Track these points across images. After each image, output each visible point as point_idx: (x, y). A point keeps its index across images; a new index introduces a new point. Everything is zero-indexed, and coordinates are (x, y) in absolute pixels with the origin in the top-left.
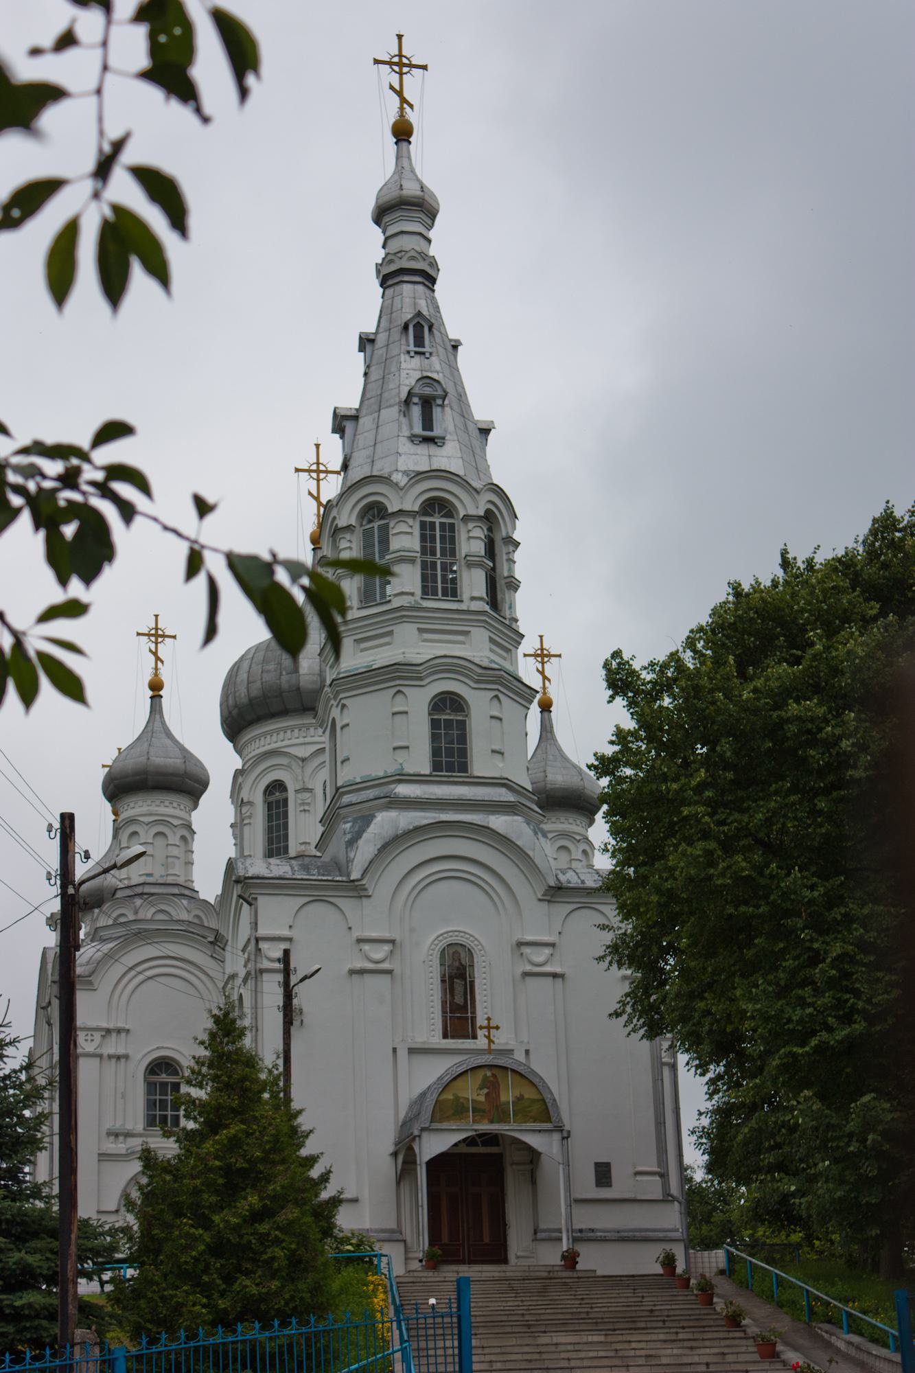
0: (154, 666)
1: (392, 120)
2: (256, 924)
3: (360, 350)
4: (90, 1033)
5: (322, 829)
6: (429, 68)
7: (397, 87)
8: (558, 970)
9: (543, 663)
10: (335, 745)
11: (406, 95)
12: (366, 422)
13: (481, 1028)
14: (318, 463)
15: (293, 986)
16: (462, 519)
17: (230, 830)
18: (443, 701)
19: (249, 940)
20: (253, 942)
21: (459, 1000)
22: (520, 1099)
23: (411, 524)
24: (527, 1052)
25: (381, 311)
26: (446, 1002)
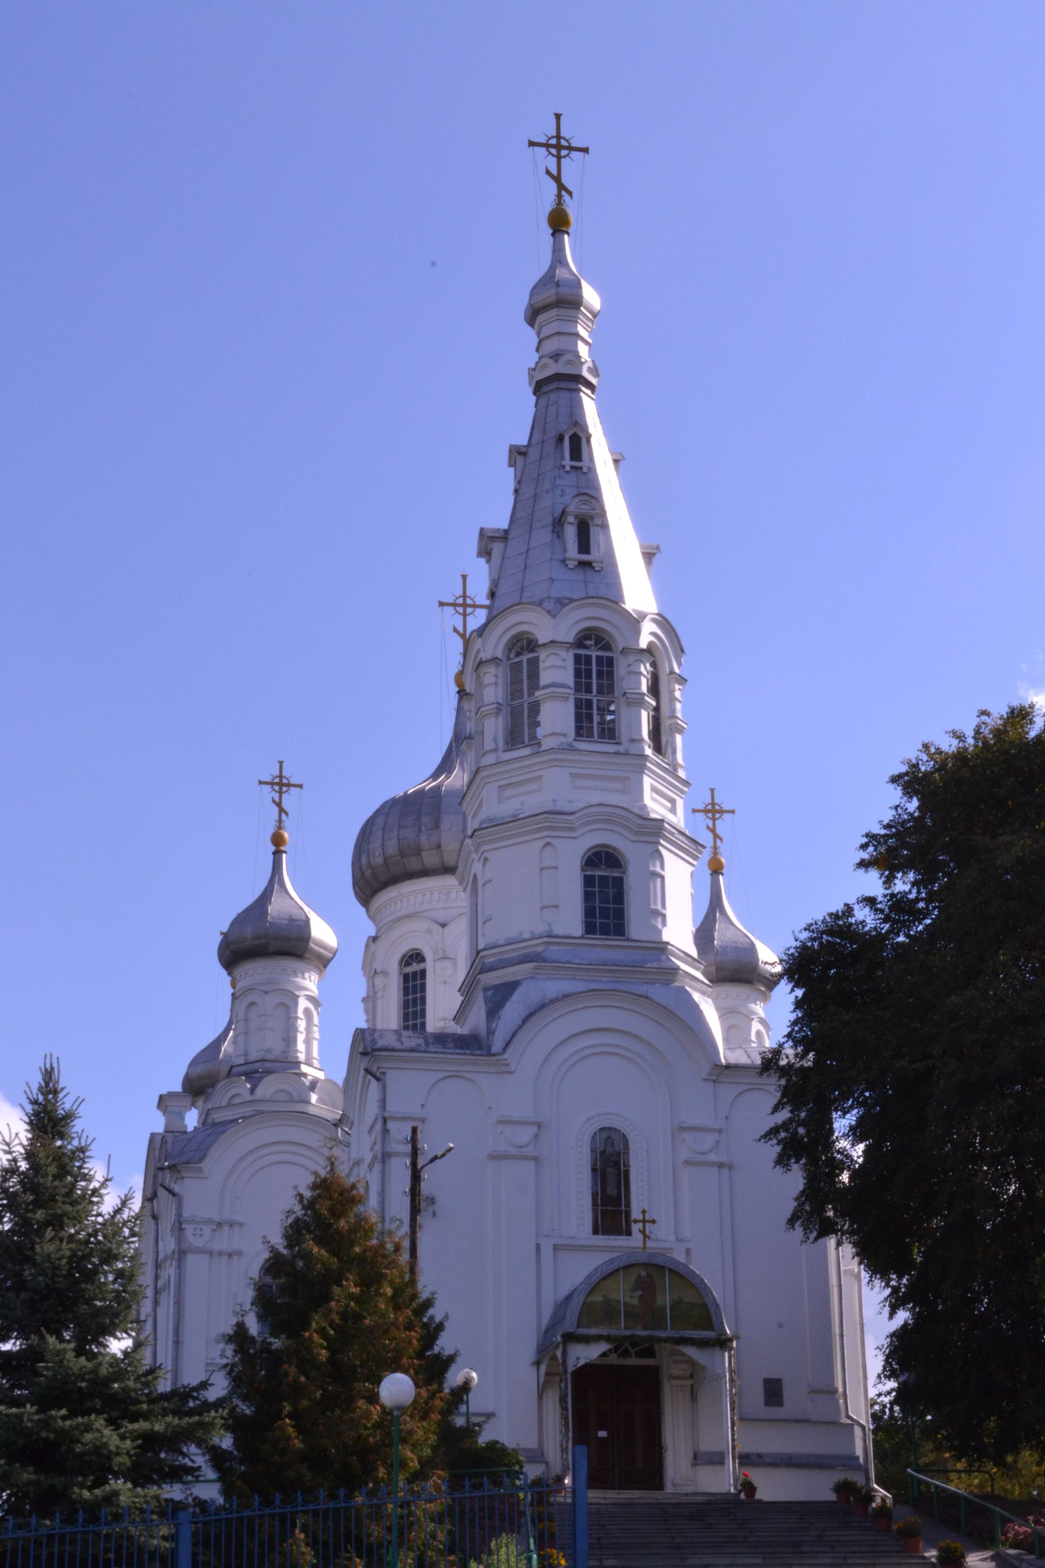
0: (277, 818)
1: (548, 209)
2: (384, 1102)
3: (510, 465)
4: (198, 1227)
5: (462, 998)
6: (590, 150)
7: (554, 172)
8: (723, 1158)
9: (714, 819)
10: (477, 905)
11: (565, 180)
12: (516, 546)
13: (636, 1221)
14: (464, 596)
15: (422, 1168)
16: (621, 652)
17: (362, 1005)
18: (598, 854)
19: (376, 1119)
20: (380, 1122)
21: (611, 1191)
22: (676, 1305)
23: (564, 657)
24: (688, 1251)
25: (534, 422)
26: (597, 1194)
